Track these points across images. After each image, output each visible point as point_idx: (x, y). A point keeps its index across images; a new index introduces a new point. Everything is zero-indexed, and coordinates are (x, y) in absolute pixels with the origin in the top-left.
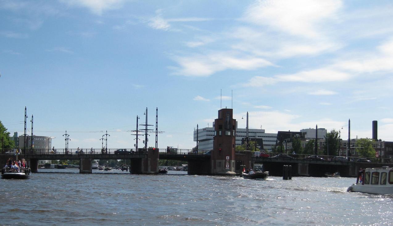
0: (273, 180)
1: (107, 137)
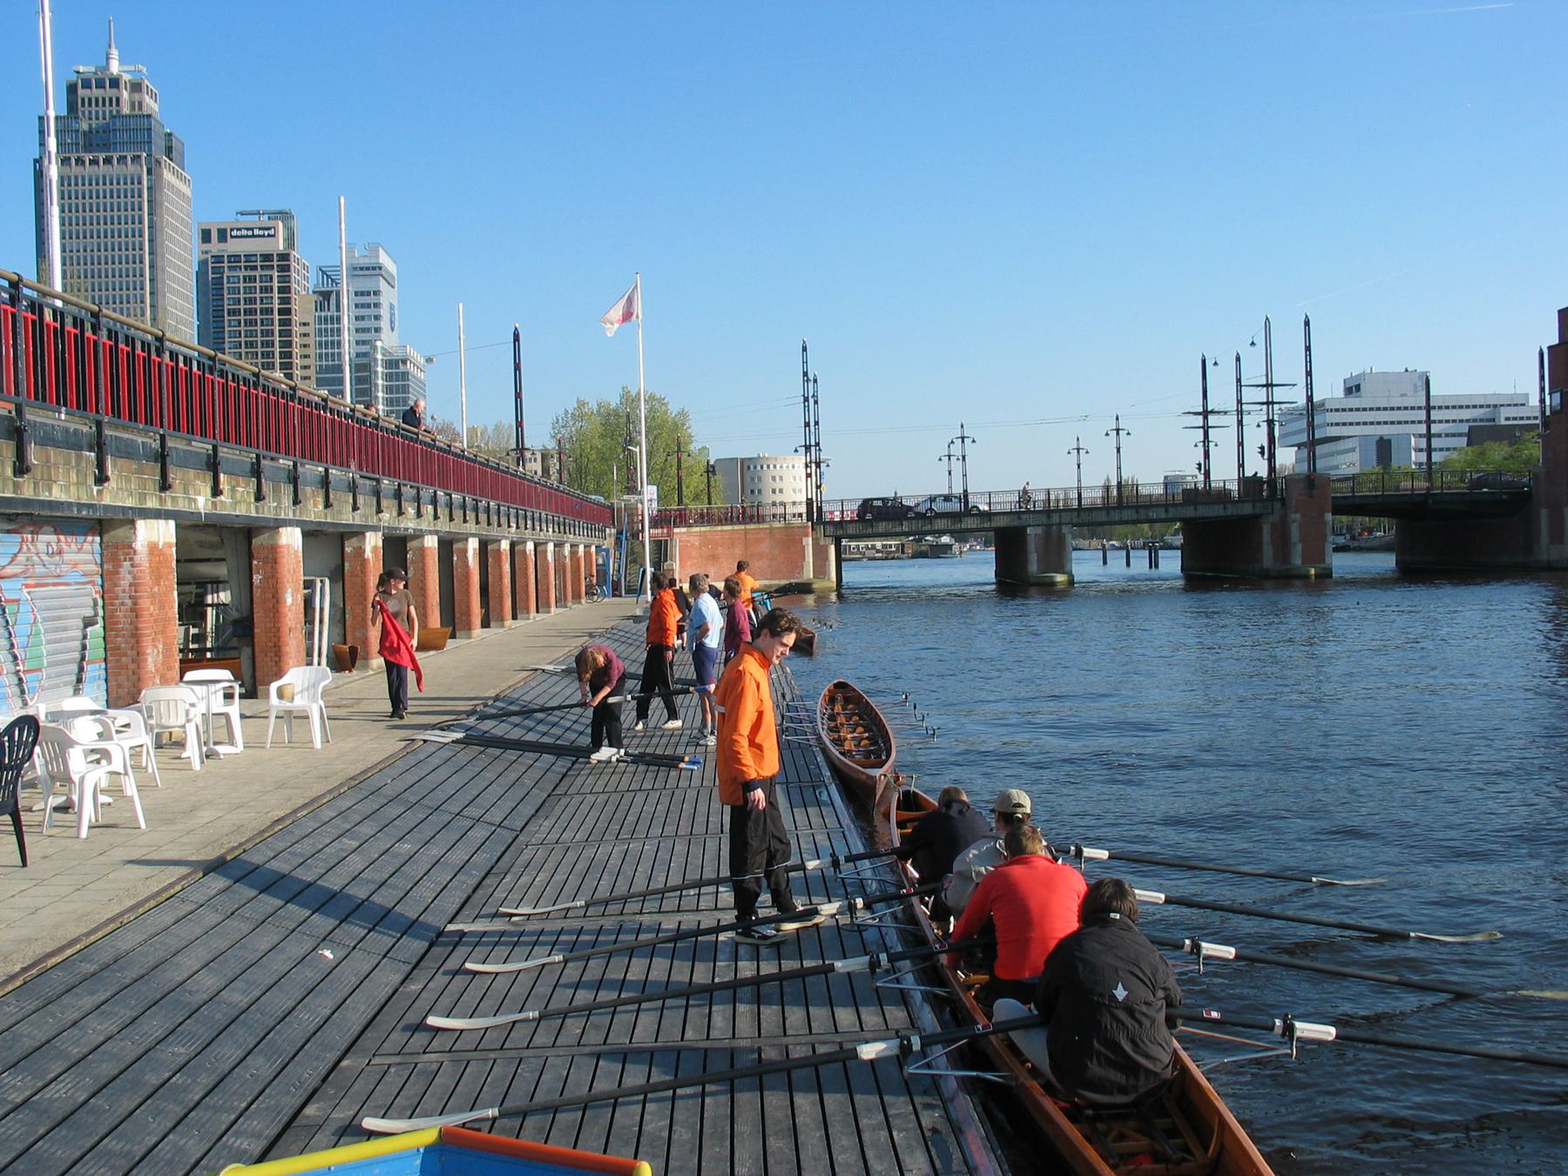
0: (209, 630)
1: (963, 448)
